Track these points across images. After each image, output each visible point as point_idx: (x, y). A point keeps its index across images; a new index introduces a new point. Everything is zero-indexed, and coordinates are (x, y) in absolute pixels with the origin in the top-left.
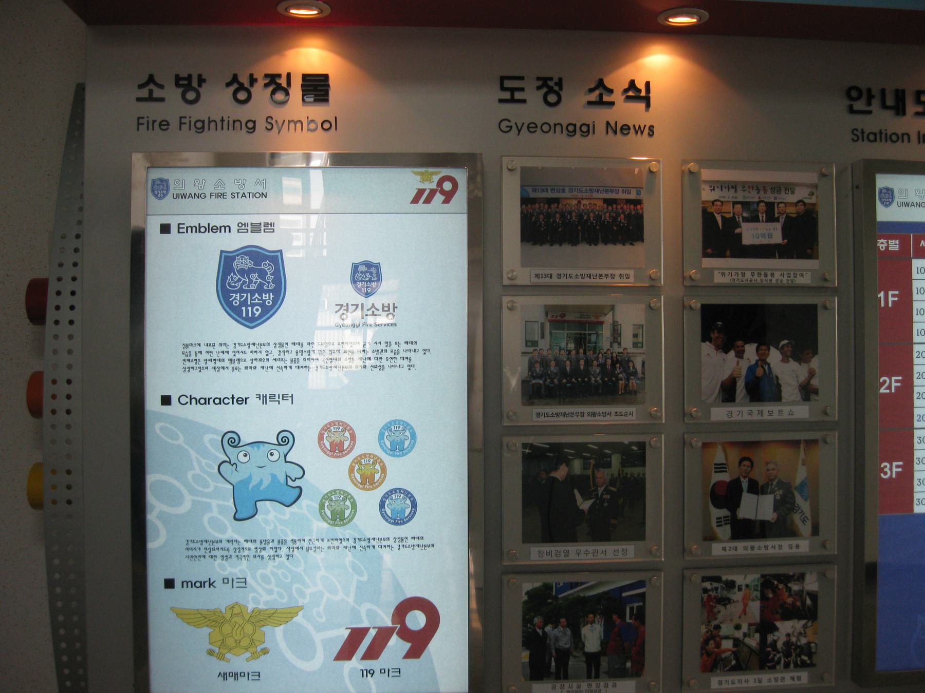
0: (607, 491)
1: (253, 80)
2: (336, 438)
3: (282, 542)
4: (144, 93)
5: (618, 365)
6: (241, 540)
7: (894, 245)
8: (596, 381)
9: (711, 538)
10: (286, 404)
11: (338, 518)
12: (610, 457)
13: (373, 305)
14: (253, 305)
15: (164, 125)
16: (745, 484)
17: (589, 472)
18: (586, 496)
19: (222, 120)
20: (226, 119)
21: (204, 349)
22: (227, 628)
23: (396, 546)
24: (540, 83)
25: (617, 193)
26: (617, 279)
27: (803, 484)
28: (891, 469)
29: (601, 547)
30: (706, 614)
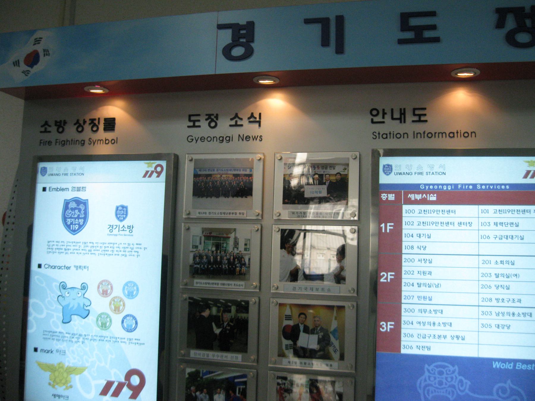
0: (228, 324)
1: (85, 122)
2: (105, 288)
3: (80, 335)
4: (233, 123)
5: (236, 260)
6: (65, 332)
7: (392, 197)
8: (225, 267)
9: (282, 355)
10: (85, 270)
11: (104, 326)
12: (230, 307)
13: (124, 226)
14: (75, 224)
15: (50, 143)
16: (302, 328)
17: (220, 314)
18: (218, 326)
19: (390, 133)
20: (459, 131)
21: (55, 243)
22: (56, 374)
23: (128, 342)
24: (207, 117)
25: (240, 171)
26: (238, 215)
27: (335, 330)
28: (387, 326)
29: (225, 354)
30: (278, 397)
